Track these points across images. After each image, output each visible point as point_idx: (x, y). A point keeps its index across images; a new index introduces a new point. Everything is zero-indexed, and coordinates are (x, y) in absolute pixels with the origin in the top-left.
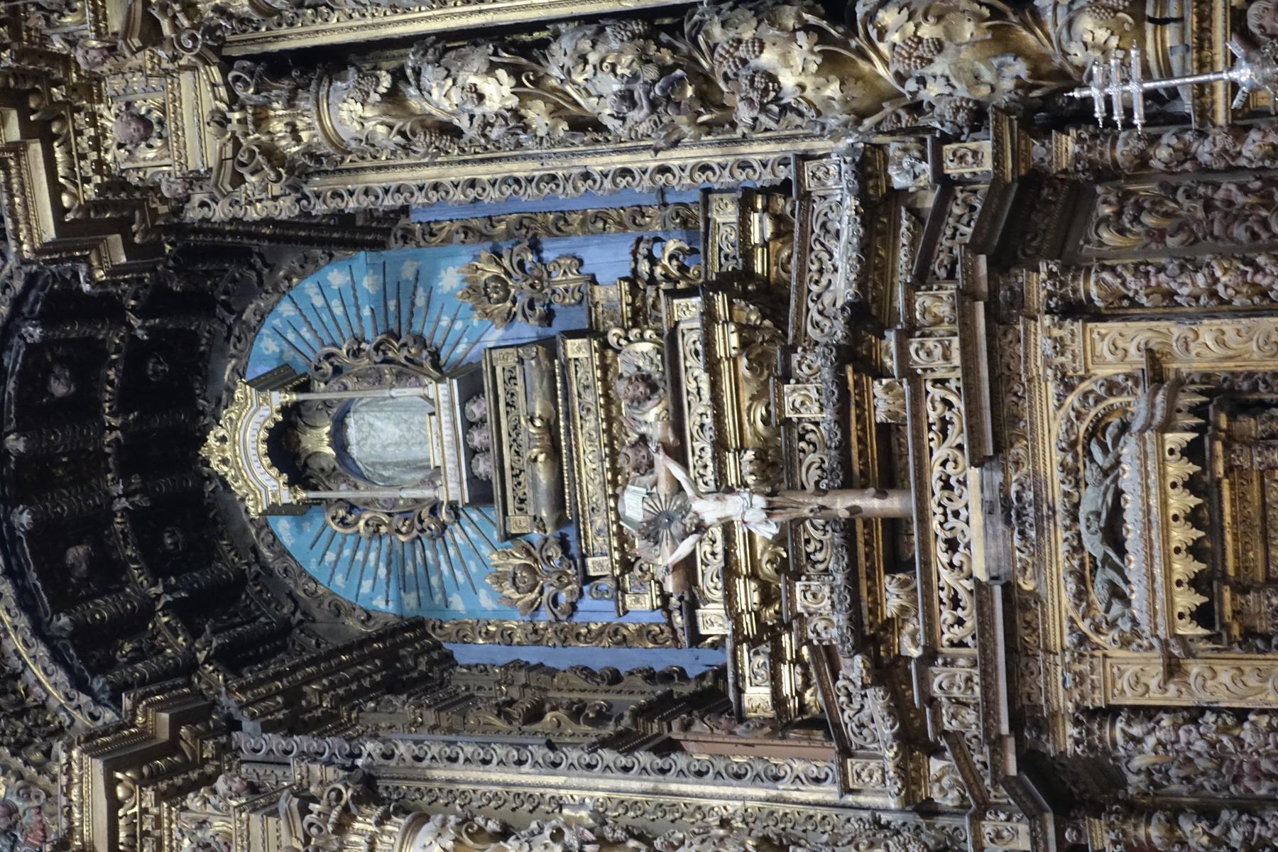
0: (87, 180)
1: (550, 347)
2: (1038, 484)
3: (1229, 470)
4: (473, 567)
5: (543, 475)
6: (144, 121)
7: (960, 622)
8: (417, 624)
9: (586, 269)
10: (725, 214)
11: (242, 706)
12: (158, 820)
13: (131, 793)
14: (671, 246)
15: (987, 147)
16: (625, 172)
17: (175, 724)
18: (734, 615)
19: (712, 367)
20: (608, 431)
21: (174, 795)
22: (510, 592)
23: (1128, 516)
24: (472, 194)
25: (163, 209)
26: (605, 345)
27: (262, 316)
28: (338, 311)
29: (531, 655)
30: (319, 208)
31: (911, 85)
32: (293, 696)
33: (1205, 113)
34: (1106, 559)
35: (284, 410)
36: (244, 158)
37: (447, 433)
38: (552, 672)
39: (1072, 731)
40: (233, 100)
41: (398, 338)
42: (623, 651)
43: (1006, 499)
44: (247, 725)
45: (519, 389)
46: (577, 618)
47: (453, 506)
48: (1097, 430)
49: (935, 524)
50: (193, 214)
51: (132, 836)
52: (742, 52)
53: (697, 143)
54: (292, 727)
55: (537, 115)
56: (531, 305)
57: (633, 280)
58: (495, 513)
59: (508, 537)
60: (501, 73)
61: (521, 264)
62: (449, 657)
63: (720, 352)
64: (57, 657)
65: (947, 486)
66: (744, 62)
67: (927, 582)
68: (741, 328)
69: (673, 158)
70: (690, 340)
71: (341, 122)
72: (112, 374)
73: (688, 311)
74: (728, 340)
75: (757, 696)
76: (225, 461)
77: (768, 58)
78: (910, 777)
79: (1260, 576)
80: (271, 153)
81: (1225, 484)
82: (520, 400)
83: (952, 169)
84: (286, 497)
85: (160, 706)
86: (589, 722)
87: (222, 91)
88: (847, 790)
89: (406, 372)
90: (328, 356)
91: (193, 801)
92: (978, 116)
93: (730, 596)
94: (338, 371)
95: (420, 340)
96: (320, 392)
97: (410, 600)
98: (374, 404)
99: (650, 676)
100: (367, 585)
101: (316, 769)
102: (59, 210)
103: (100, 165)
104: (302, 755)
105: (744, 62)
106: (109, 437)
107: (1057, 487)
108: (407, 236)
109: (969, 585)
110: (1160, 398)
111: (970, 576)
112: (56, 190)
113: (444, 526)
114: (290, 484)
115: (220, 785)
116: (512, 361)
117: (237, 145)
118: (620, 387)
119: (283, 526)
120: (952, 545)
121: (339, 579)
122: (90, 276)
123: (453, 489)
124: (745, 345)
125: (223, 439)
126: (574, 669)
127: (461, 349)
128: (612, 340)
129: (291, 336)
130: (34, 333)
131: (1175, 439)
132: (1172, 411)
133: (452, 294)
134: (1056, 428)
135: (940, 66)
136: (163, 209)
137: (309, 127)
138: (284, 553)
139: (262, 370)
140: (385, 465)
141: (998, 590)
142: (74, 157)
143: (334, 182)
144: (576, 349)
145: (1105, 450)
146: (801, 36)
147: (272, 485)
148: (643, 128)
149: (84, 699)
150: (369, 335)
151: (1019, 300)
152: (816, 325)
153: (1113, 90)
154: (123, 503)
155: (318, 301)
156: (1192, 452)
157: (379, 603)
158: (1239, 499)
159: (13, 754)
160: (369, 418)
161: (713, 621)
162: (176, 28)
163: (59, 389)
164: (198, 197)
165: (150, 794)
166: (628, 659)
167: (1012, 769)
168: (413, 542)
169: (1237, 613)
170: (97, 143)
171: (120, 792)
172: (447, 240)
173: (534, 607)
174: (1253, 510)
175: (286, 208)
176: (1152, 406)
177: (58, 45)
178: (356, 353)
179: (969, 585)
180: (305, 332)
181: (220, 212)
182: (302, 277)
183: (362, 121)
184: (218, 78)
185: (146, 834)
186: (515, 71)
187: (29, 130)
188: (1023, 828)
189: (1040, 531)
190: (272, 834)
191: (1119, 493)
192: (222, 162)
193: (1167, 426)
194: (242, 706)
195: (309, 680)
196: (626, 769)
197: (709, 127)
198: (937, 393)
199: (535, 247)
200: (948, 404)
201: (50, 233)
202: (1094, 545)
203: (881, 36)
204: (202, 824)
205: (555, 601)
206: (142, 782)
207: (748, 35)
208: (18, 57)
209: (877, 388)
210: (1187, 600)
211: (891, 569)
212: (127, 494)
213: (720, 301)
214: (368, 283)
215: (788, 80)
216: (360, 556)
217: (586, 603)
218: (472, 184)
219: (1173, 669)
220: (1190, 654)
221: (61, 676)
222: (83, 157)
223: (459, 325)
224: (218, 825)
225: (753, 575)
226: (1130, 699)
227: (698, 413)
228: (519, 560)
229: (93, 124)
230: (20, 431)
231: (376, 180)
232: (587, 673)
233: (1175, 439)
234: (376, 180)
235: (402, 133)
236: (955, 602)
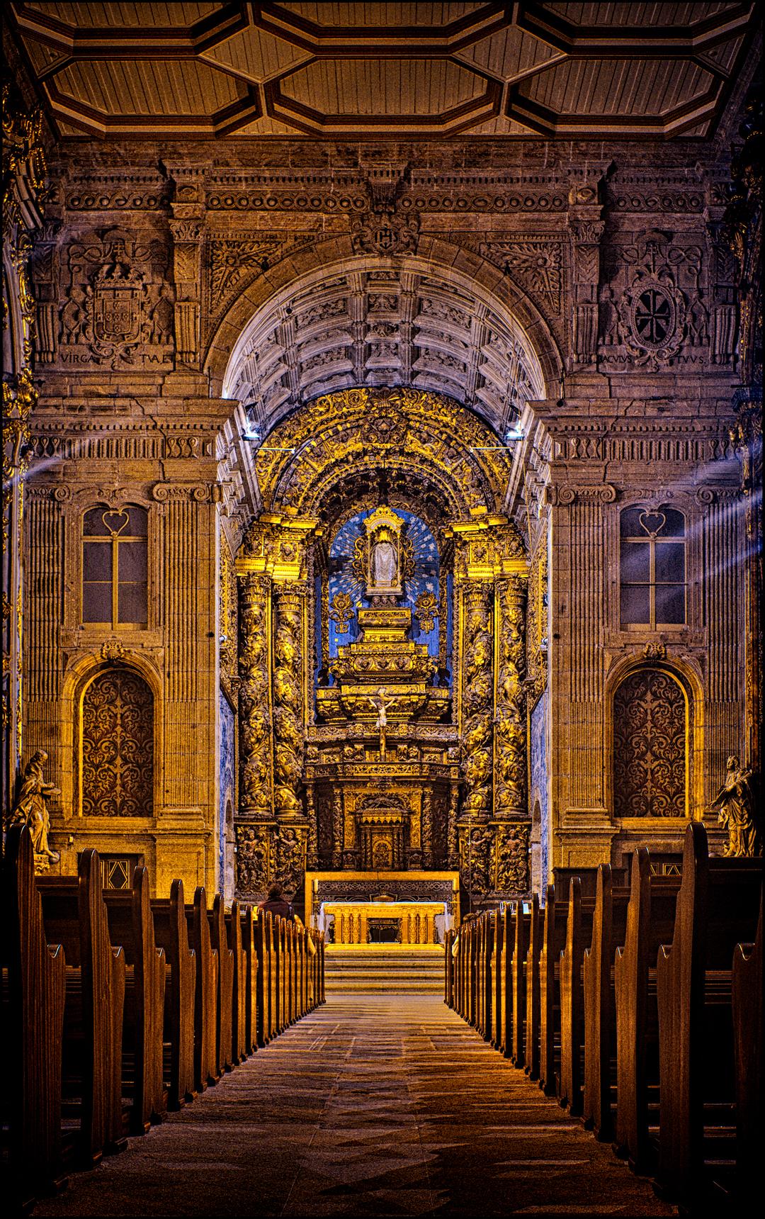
2: (390, 788)
5: (375, 622)
15: (456, 777)
19: (408, 694)
33: (459, 822)
48: (400, 802)
55: (472, 669)
68: (417, 703)
74: (415, 698)
75: (322, 694)
77: (480, 728)
78: (314, 744)
79: (69, 394)
83: (452, 769)
92: (462, 774)
93: (352, 695)
107: (389, 792)
124: (413, 703)
131: (400, 819)
134: (400, 792)
135: (474, 767)
155: (425, 539)
156: (398, 822)
186: (483, 665)
209: (406, 746)
215: (474, 732)
219: (351, 813)
233: (400, 819)
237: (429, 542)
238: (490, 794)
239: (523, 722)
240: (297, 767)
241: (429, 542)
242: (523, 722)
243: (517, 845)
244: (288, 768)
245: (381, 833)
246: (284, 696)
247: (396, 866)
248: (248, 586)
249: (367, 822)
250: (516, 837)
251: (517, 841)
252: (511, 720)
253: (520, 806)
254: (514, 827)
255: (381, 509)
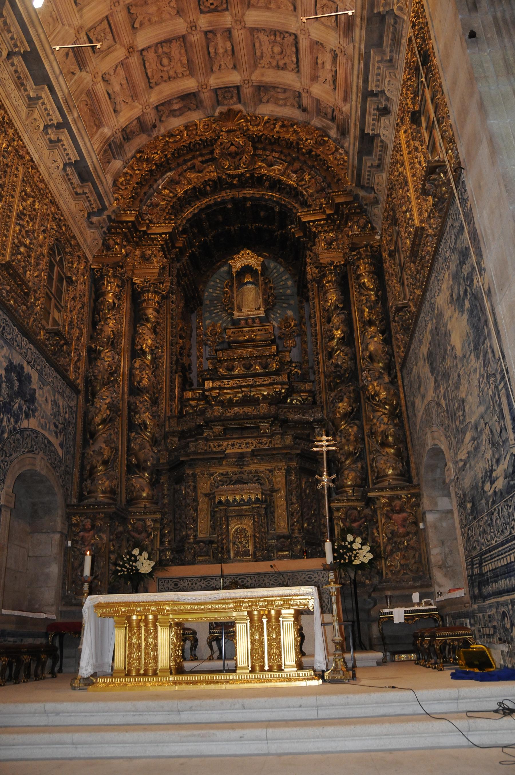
0: (316, 229)
1: (273, 342)
2: (248, 465)
3: (253, 508)
4: (216, 319)
6: (331, 244)
7: (215, 447)
8: (201, 304)
9: (293, 349)
10: (307, 386)
11: (183, 263)
12: (156, 245)
13: (163, 238)
14: (299, 372)
16: (318, 363)
17: (180, 248)
18: (210, 389)
20: (253, 356)
21: (162, 249)
22: (210, 328)
23: (242, 485)
24: (313, 325)
25: (309, 246)
26: (275, 356)
27: (280, 263)
28: (281, 283)
29: (194, 333)
30: (309, 286)
31: (339, 434)
32: (185, 275)
34: (231, 481)
35: (257, 270)
36: (322, 269)
37: (250, 313)
38: (190, 340)
39: (191, 473)
40: (336, 267)
41: (275, 299)
42: (196, 358)
43: (244, 457)
44: (178, 265)
45: (263, 332)
46: (204, 346)
47: (232, 314)
49: (237, 441)
50: (308, 253)
51: (153, 238)
52: (347, 394)
53: (325, 382)
54: (178, 276)
56: (283, 334)
57: (291, 362)
58: (229, 326)
59: (225, 329)
60: (343, 335)
61: (294, 332)
62: (193, 312)
63: (275, 386)
64: (195, 215)
65: (246, 444)
66: (345, 394)
67: (224, 439)
69: (322, 376)
70: (278, 379)
71: (331, 294)
72: (265, 226)
73: (284, 378)
76: (243, 254)
80: (324, 276)
81: (250, 507)
82: (260, 333)
84: (234, 270)
85: (184, 244)
86: (180, 352)
87: (338, 264)
88: (169, 418)
89: (266, 302)
90: (270, 281)
91: (161, 254)
93: (214, 388)
94: (266, 284)
95: (274, 305)
96: (261, 279)
97: (207, 302)
98: (257, 293)
99: (190, 365)
100: (211, 290)
101: (169, 284)
102: (309, 222)
103: (320, 232)
104: (172, 280)
105: (345, 394)
106: (249, 225)
108: (301, 302)
109: (224, 449)
110: (268, 492)
111: (226, 449)
112: (314, 221)
113: (227, 311)
114: (237, 271)
115: (165, 260)
116: (270, 330)
117: (325, 267)
118: (265, 359)
119: (225, 268)
120: (233, 445)
121: (212, 283)
122: (293, 228)
123: (237, 315)
125: (248, 254)
126: (191, 345)
127: (272, 316)
128: (276, 358)
129: (275, 271)
130: (277, 209)
132: (266, 495)
133: (287, 314)
134: (261, 469)
135: (344, 440)
136: (309, 246)
137: (330, 286)
138: (219, 268)
139: (266, 263)
140: (242, 295)
141: (223, 456)
142: (322, 226)
143: (316, 289)
144: (274, 347)
145: (257, 480)
146: (351, 408)
147: (237, 267)
148: (330, 369)
149: (184, 222)
150: (275, 292)
151: (291, 459)
152: (282, 411)
153: (324, 443)
154: (232, 229)
155: (284, 278)
157: (206, 294)
158: (246, 510)
159: (171, 206)
160: (254, 291)
161: (209, 384)
162: (354, 255)
163: (262, 214)
164: (312, 254)
165: (163, 243)
166: (194, 358)
167: (181, 459)
168: (222, 303)
169: (221, 510)
170: (326, 232)
171: (164, 236)
172: (300, 313)
173: (206, 335)
174: (244, 513)
175: (309, 277)
176: (267, 491)
177: (350, 224)
178: (271, 288)
179: (224, 449)
180: (276, 274)
181: (308, 260)
182: (290, 274)
183: (332, 300)
184: (342, 263)
185: (153, 242)
187: (329, 216)
188: (165, 461)
189: (237, 465)
190: (154, 275)
191: (247, 483)
192: (321, 264)
193: (263, 494)
194: (183, 263)
195: (189, 280)
196: (172, 363)
197: (330, 385)
198: (268, 441)
199: (298, 335)
200: (266, 444)
201: (304, 220)
202: (235, 478)
203: (350, 427)
204: (155, 256)
205: (209, 340)
206: (166, 241)
207: (352, 395)
208: (347, 214)
210: (223, 499)
211: (225, 429)
212: (235, 230)
213: (287, 386)
214: (289, 291)
216: (218, 289)
217: (208, 349)
218: (316, 325)
220: (210, 499)
221: (190, 216)
222: (322, 228)
223: (278, 315)
224: (156, 260)
225: (219, 394)
226: (199, 486)
227: (259, 381)
228: (219, 331)
229: (330, 230)
230: (252, 205)
231: (316, 301)
232: (190, 349)
234: (316, 301)
235: (328, 309)
236: (219, 446)
237: (287, 279)
238: (364, 469)
239: (393, 382)
240: (151, 454)
241: (287, 279)
242: (393, 382)
243: (405, 520)
244: (142, 455)
245: (240, 516)
246: (139, 383)
247: (258, 554)
248: (102, 277)
249: (220, 502)
250: (401, 510)
251: (404, 515)
252: (381, 381)
253: (401, 475)
254: (399, 498)
255: (242, 252)
